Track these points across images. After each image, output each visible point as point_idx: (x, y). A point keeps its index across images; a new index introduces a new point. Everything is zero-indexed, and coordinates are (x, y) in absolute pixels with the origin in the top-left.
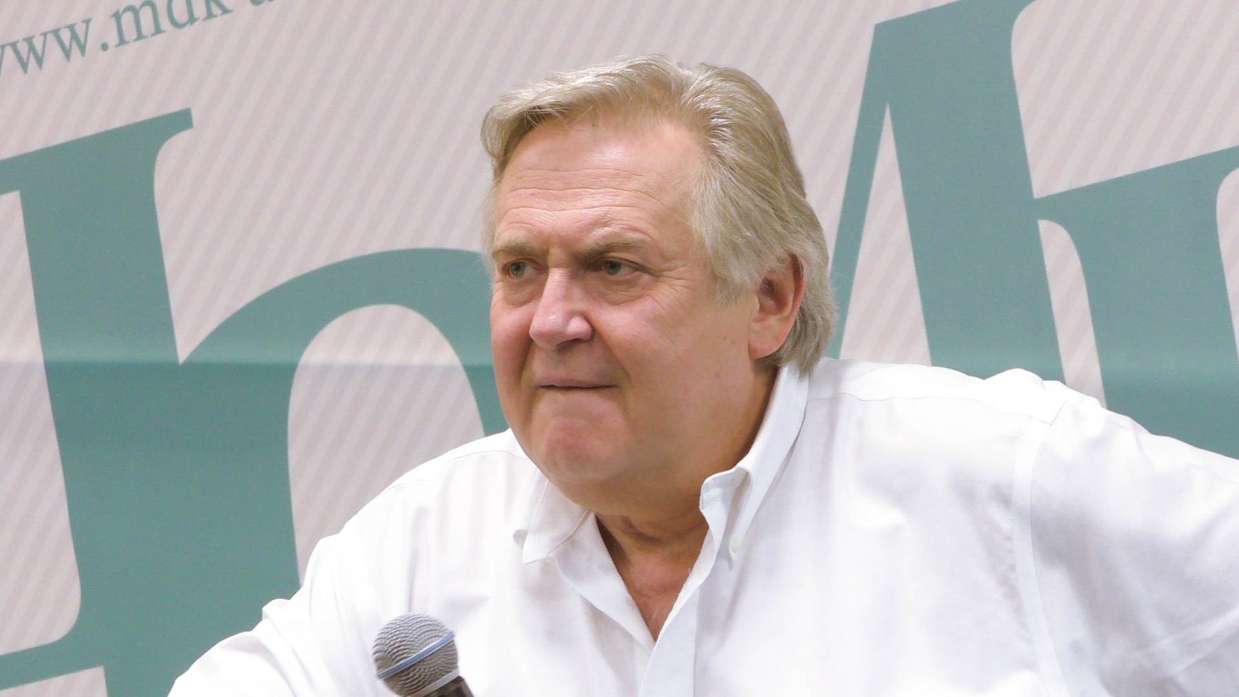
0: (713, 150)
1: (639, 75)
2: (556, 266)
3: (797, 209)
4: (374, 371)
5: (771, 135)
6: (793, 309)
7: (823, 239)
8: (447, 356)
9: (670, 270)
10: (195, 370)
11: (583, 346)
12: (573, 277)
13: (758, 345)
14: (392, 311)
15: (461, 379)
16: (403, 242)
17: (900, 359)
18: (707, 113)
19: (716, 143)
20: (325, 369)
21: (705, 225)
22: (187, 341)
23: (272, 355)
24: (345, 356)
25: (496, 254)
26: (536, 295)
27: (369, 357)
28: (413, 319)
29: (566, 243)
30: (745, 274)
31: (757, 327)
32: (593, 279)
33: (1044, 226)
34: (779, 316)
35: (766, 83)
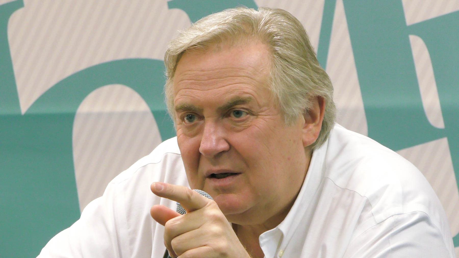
0: (275, 52)
1: (237, 22)
2: (208, 117)
3: (318, 73)
4: (111, 115)
5: (301, 40)
6: (320, 119)
7: (330, 82)
8: (143, 107)
9: (262, 111)
10: (29, 116)
11: (225, 155)
12: (217, 122)
13: (306, 140)
14: (118, 88)
15: (150, 118)
16: (122, 56)
18: (271, 35)
19: (277, 48)
20: (88, 115)
21: (277, 89)
22: (25, 105)
23: (63, 109)
24: (97, 109)
25: (178, 110)
26: (200, 131)
27: (108, 108)
28: (128, 90)
29: (210, 105)
30: (298, 107)
31: (305, 131)
32: (226, 121)
33: (412, 38)
34: (314, 124)
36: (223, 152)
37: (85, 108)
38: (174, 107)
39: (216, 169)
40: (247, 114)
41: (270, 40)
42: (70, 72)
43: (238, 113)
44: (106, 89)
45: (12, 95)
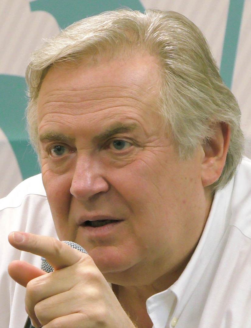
0: (166, 66)
5: (200, 51)
11: (103, 198)
12: (92, 155)
13: (207, 178)
17: (248, 158)
18: (161, 44)
19: (169, 61)
26: (71, 167)
31: (204, 166)
34: (216, 158)
35: (198, 23)
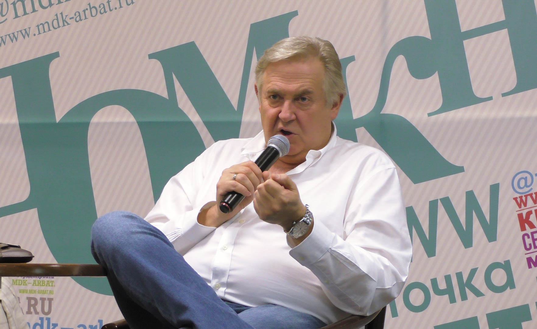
4: (112, 123)
8: (132, 119)
10: (60, 124)
14: (116, 107)
15: (136, 126)
20: (98, 124)
22: (59, 117)
23: (82, 120)
24: (103, 120)
27: (110, 120)
28: (123, 109)
32: (297, 103)
36: (292, 121)
37: (95, 119)
38: (264, 95)
39: (286, 129)
40: (309, 100)
41: (323, 59)
42: (87, 97)
43: (304, 99)
44: (109, 108)
45: (51, 111)
